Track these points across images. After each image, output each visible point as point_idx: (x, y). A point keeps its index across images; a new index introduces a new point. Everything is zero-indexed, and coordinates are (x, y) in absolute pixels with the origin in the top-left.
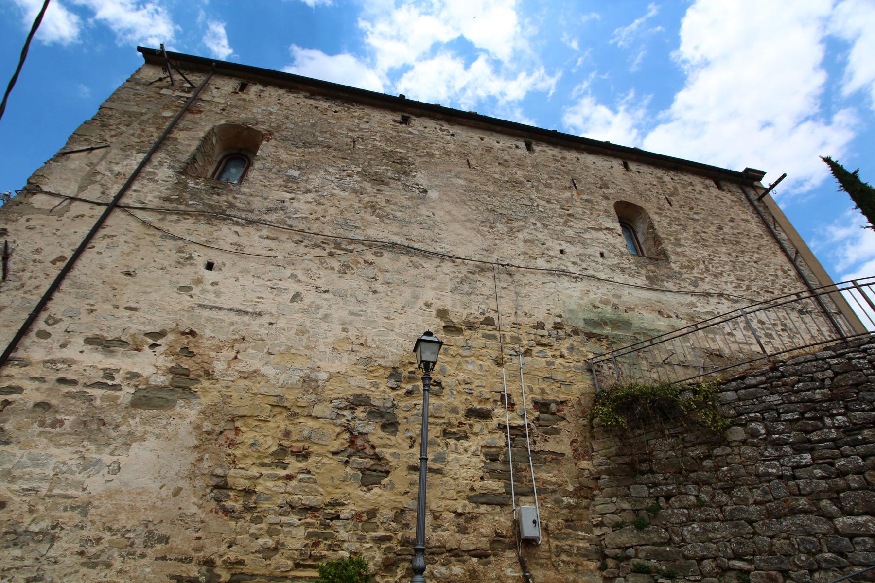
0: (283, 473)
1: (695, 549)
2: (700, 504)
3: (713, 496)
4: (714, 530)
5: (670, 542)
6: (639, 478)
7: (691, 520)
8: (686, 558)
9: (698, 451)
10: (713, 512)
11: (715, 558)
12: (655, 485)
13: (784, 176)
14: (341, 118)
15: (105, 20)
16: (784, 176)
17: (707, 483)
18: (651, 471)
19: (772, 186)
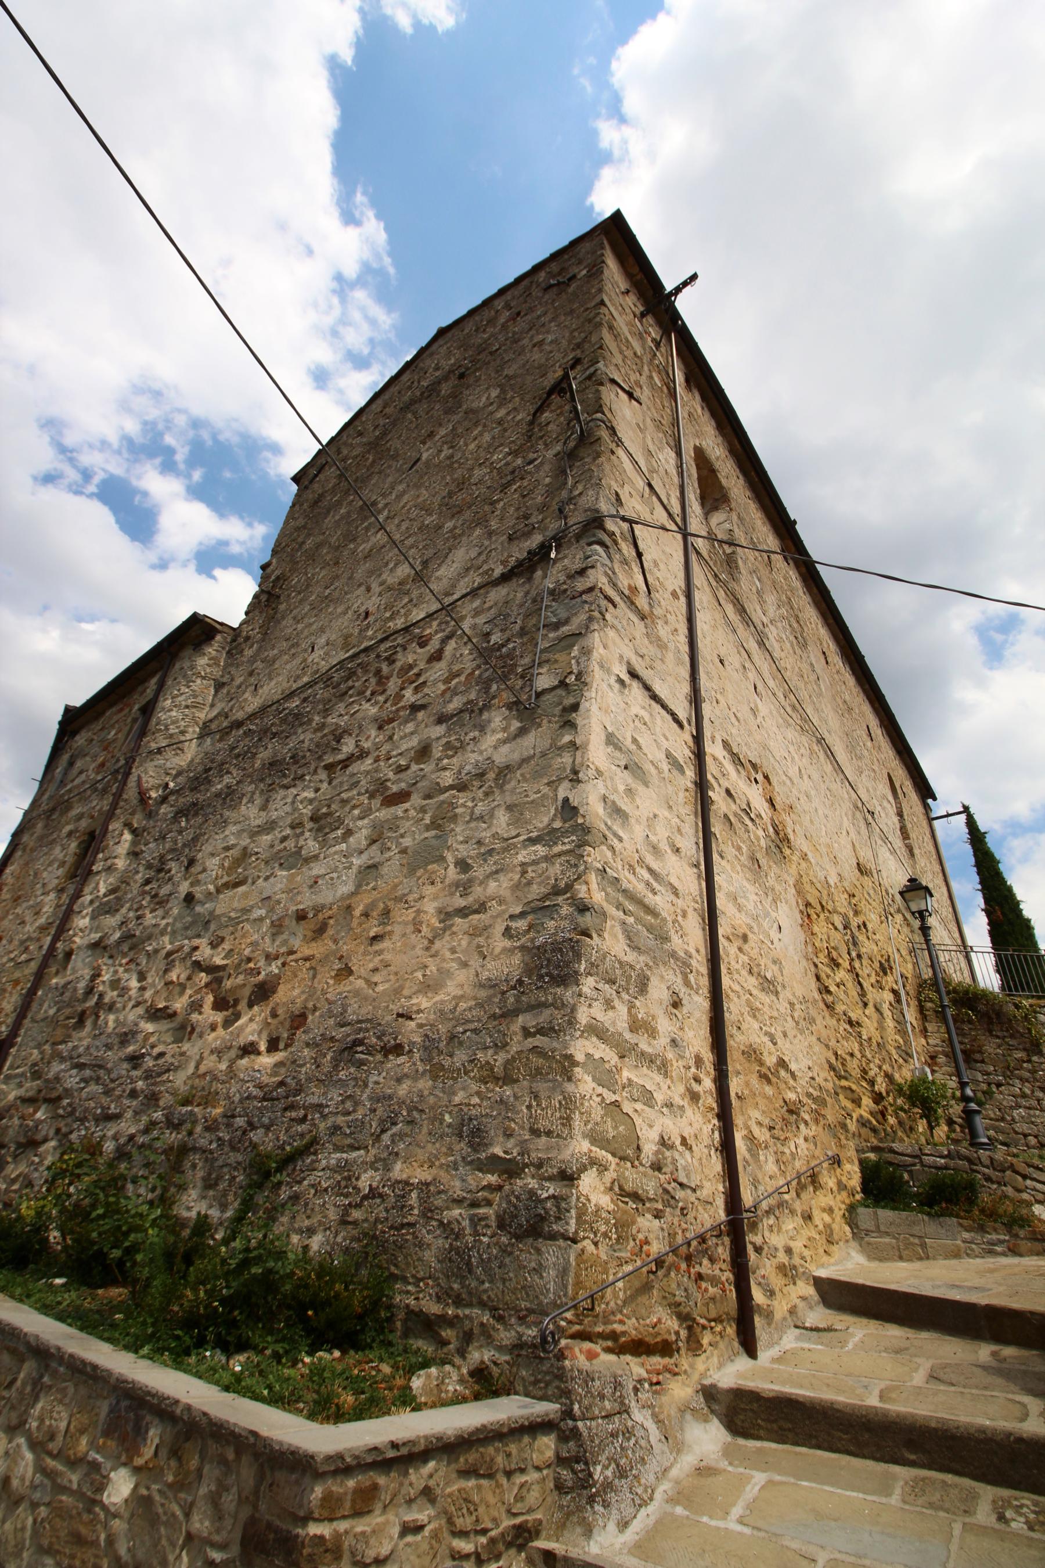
0: (651, 447)
1: (1021, 1127)
2: (1024, 1096)
3: (1033, 1092)
4: (1035, 1116)
5: (1003, 1119)
6: (973, 1064)
7: (1018, 1106)
8: (1016, 1133)
9: (1019, 1055)
10: (1034, 1103)
11: (1036, 1137)
12: (988, 1074)
13: (694, 277)
14: (457, 1169)
15: (201, 544)
16: (694, 277)
17: (1027, 1081)
18: (983, 1062)
19: (678, 290)
